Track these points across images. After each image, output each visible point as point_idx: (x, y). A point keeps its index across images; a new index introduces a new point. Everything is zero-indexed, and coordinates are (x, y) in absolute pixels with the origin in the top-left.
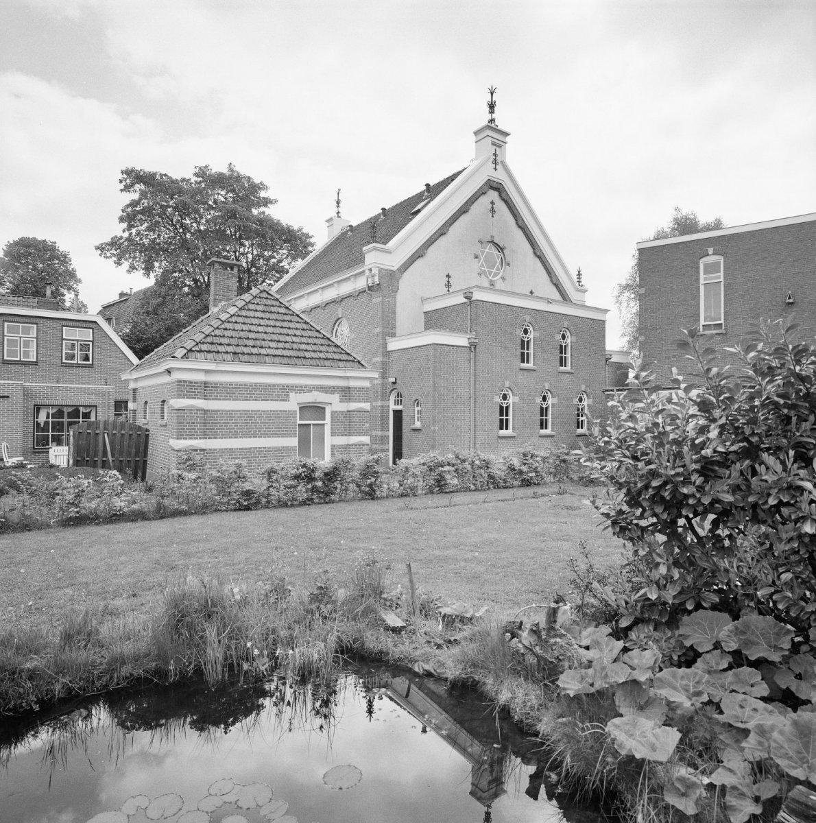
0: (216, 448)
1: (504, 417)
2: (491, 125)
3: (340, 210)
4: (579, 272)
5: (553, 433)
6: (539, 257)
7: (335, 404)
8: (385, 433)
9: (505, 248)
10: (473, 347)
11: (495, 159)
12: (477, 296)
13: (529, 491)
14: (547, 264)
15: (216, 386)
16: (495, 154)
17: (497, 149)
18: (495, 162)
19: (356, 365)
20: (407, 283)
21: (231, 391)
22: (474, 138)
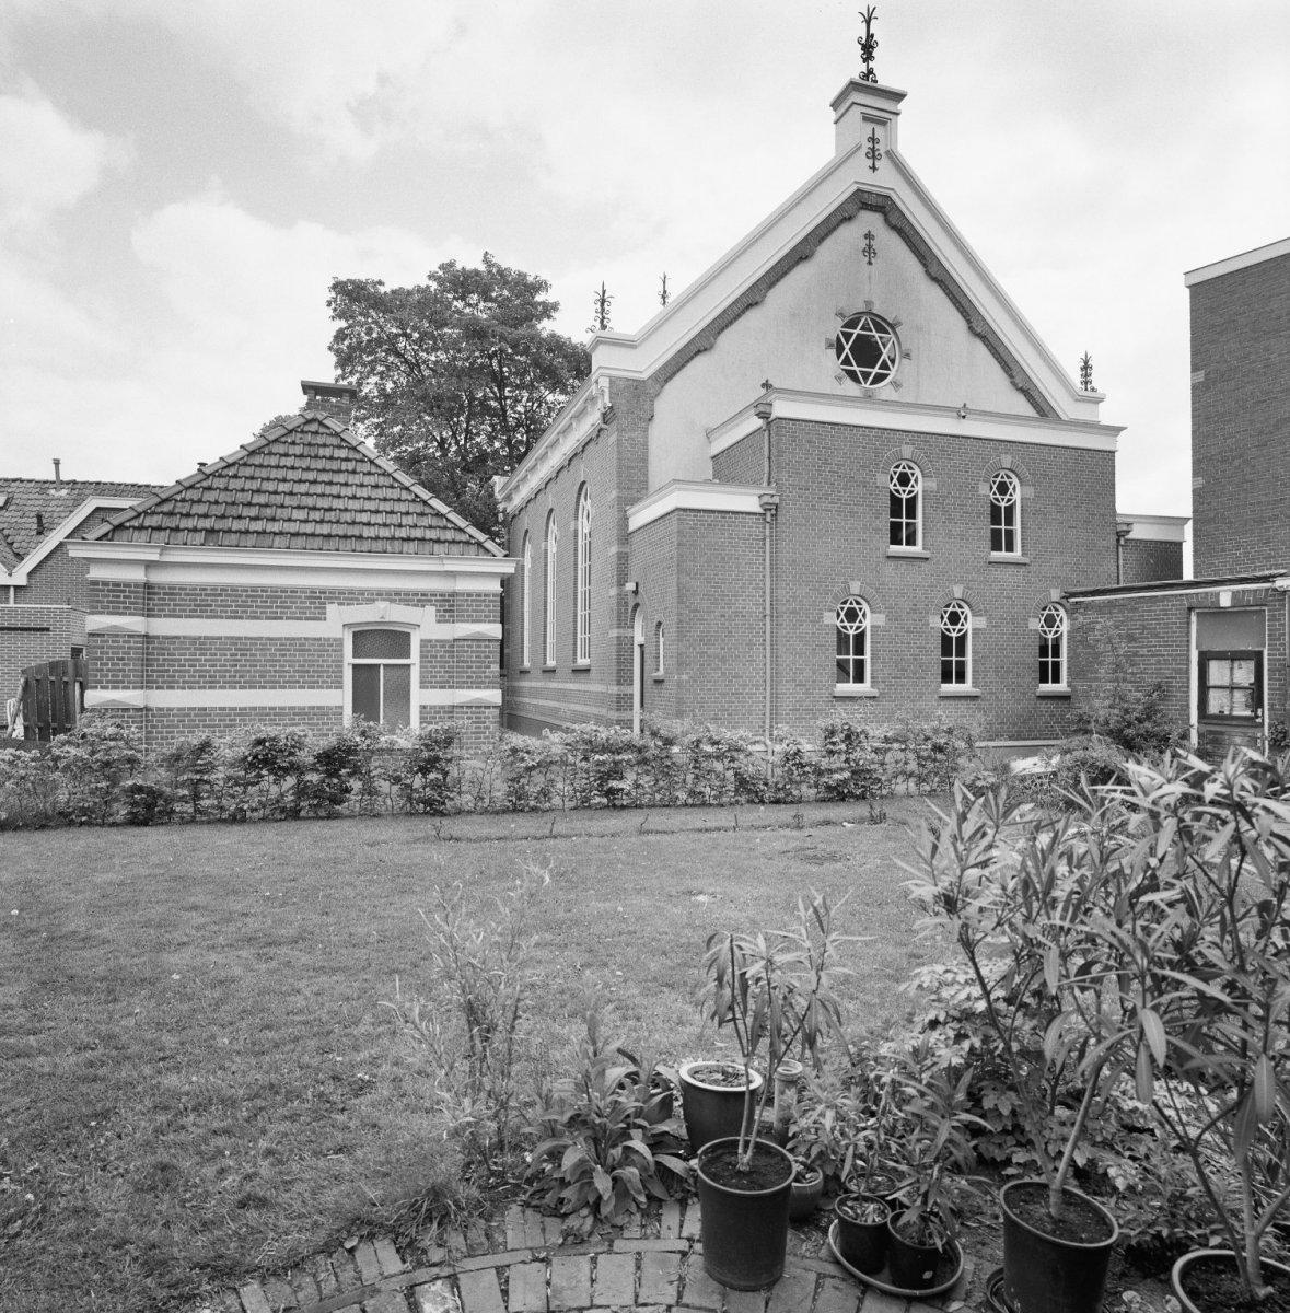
0: (172, 706)
1: (1050, 659)
2: (865, 84)
4: (1086, 362)
5: (976, 692)
6: (983, 338)
7: (426, 626)
8: (625, 689)
9: (900, 324)
10: (771, 511)
11: (873, 150)
12: (781, 409)
13: (426, 826)
14: (1001, 350)
15: (172, 591)
18: (873, 154)
19: (473, 549)
20: (671, 404)
21: (203, 602)
22: (833, 115)
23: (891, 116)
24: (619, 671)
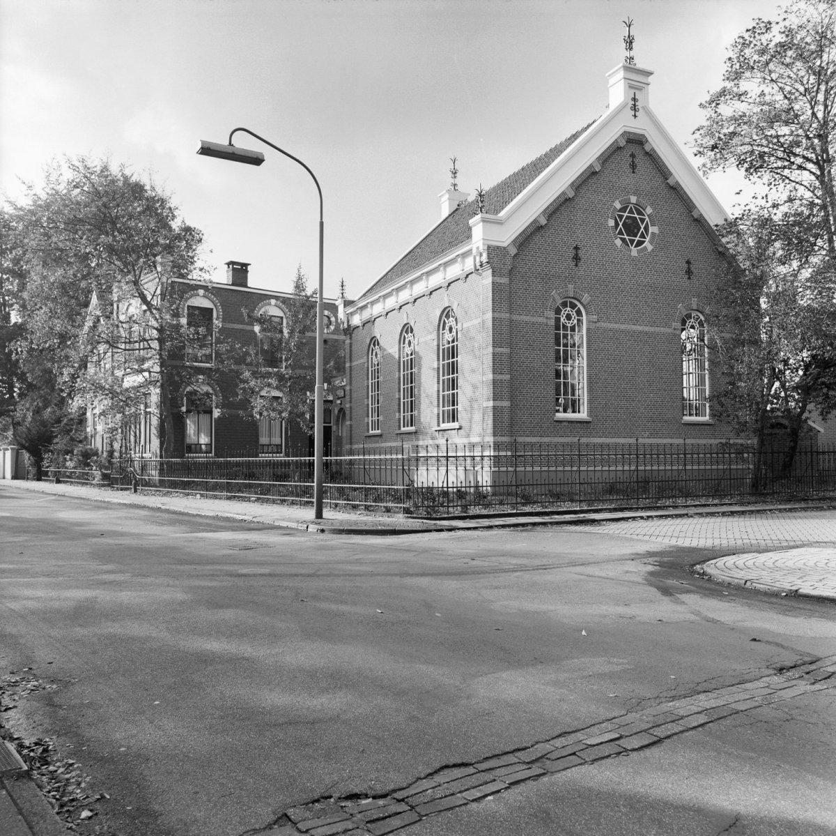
3: (457, 181)
16: (634, 99)
17: (637, 92)
18: (634, 108)
23: (644, 85)
24: (522, 557)
